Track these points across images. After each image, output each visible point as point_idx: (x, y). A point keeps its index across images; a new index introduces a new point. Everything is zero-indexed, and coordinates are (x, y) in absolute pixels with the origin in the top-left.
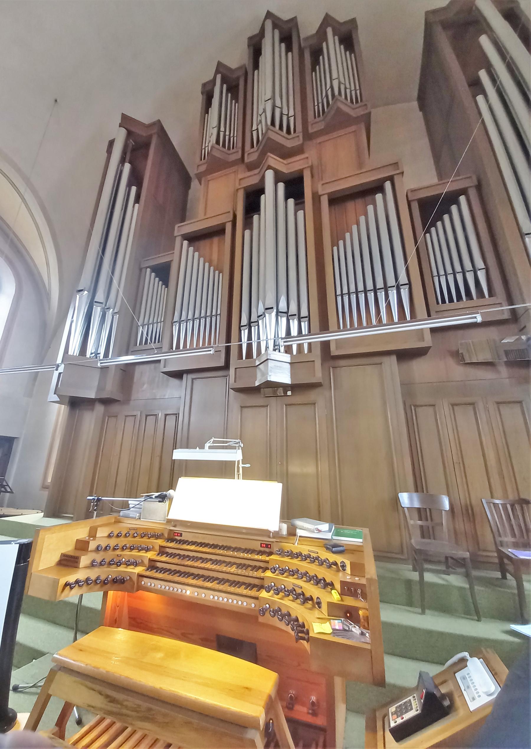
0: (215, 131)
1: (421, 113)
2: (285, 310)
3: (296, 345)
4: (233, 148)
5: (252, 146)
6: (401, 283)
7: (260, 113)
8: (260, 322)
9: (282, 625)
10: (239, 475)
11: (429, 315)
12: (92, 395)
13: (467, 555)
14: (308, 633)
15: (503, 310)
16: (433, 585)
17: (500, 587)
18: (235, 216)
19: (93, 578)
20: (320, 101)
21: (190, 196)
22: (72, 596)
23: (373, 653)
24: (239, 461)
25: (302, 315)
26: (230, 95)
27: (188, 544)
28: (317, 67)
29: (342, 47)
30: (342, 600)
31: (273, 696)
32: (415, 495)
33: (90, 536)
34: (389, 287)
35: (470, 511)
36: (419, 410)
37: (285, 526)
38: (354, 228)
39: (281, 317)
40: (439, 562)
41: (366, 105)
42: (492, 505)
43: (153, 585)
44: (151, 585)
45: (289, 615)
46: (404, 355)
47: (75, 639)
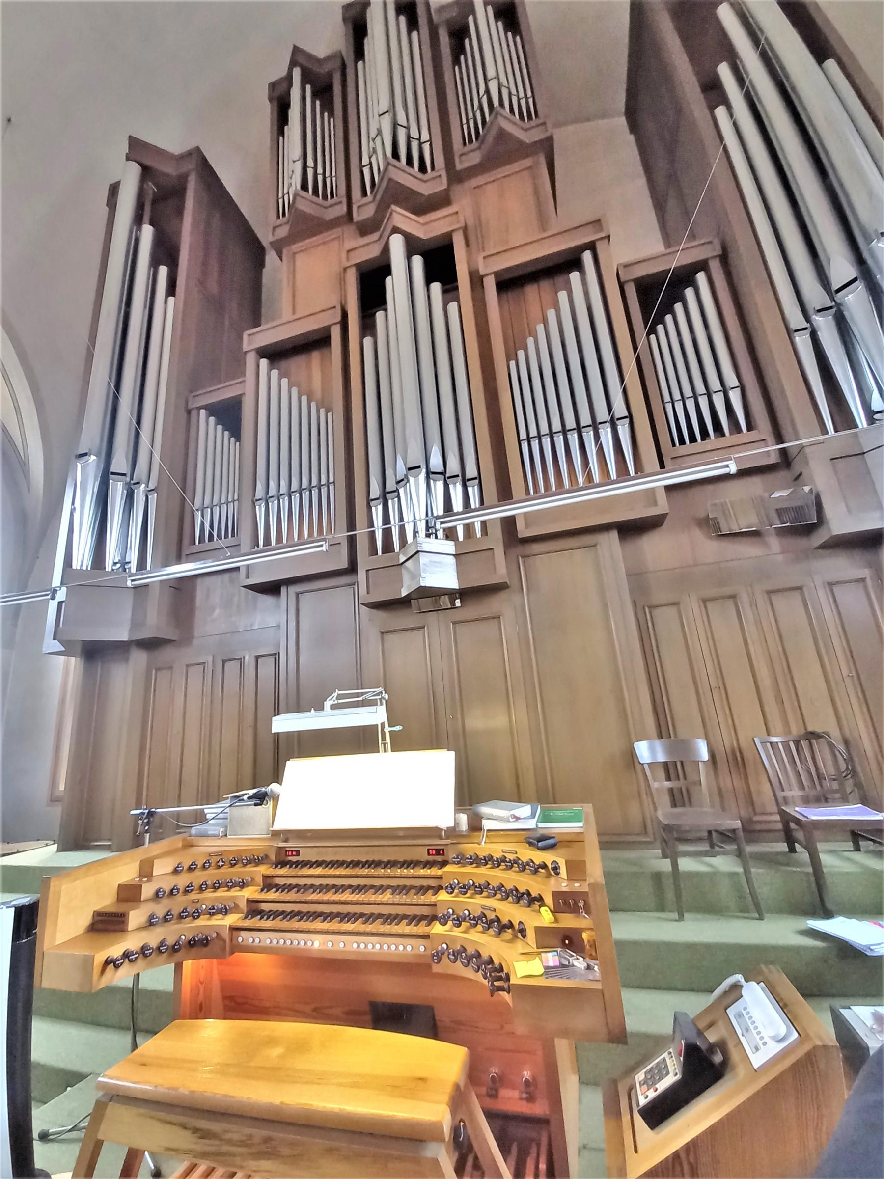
0: (298, 166)
1: (632, 138)
2: (441, 469)
3: (461, 526)
4: (332, 196)
5: (364, 194)
6: (617, 416)
7: (373, 135)
8: (401, 491)
9: (469, 973)
10: (385, 744)
11: (662, 465)
12: (123, 635)
13: (737, 824)
14: (508, 978)
15: (769, 451)
16: (691, 875)
17: (788, 865)
18: (345, 315)
19: (154, 944)
20: (471, 115)
21: (265, 280)
22: (123, 977)
23: (606, 995)
24: (383, 725)
25: (468, 476)
26: (318, 103)
27: (311, 867)
28: (462, 57)
29: (500, 24)
30: (556, 921)
31: (462, 1084)
32: (658, 744)
33: (141, 875)
34: (600, 423)
35: (739, 759)
36: (657, 612)
37: (463, 818)
38: (540, 328)
39: (435, 481)
40: (700, 840)
41: (544, 124)
42: (768, 744)
43: (257, 940)
44: (254, 941)
45: (478, 955)
46: (630, 530)
47: (135, 1046)
